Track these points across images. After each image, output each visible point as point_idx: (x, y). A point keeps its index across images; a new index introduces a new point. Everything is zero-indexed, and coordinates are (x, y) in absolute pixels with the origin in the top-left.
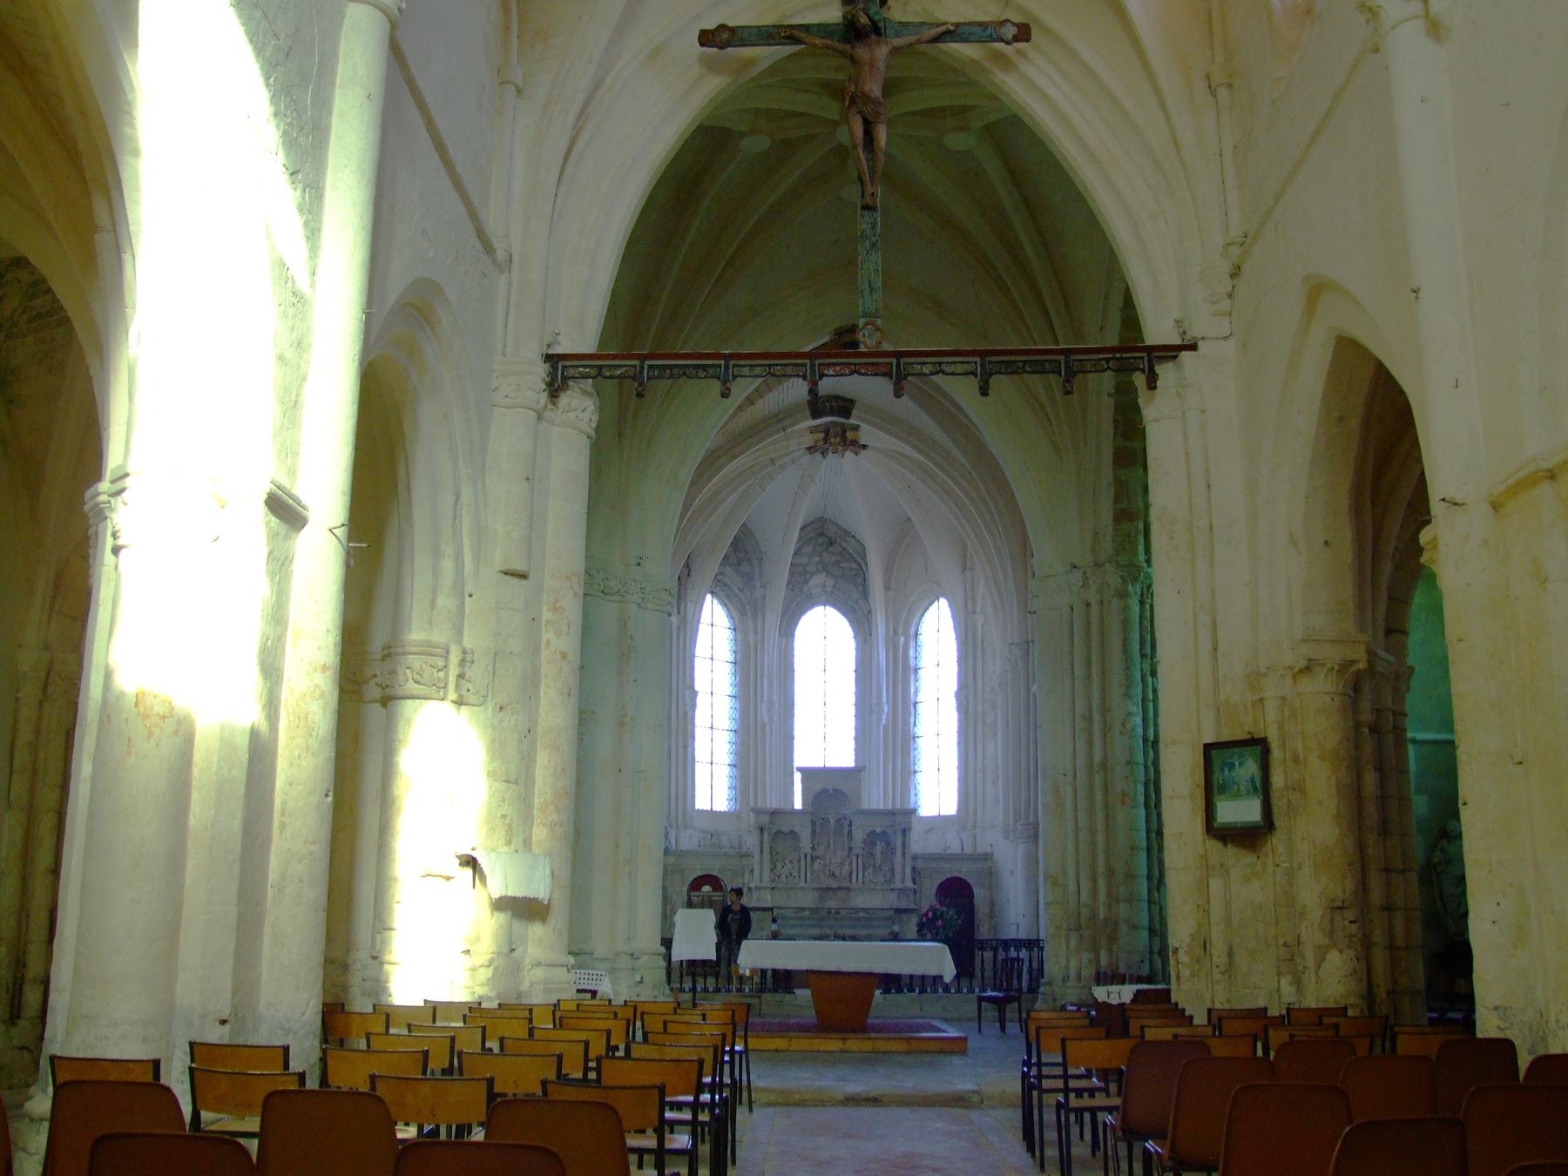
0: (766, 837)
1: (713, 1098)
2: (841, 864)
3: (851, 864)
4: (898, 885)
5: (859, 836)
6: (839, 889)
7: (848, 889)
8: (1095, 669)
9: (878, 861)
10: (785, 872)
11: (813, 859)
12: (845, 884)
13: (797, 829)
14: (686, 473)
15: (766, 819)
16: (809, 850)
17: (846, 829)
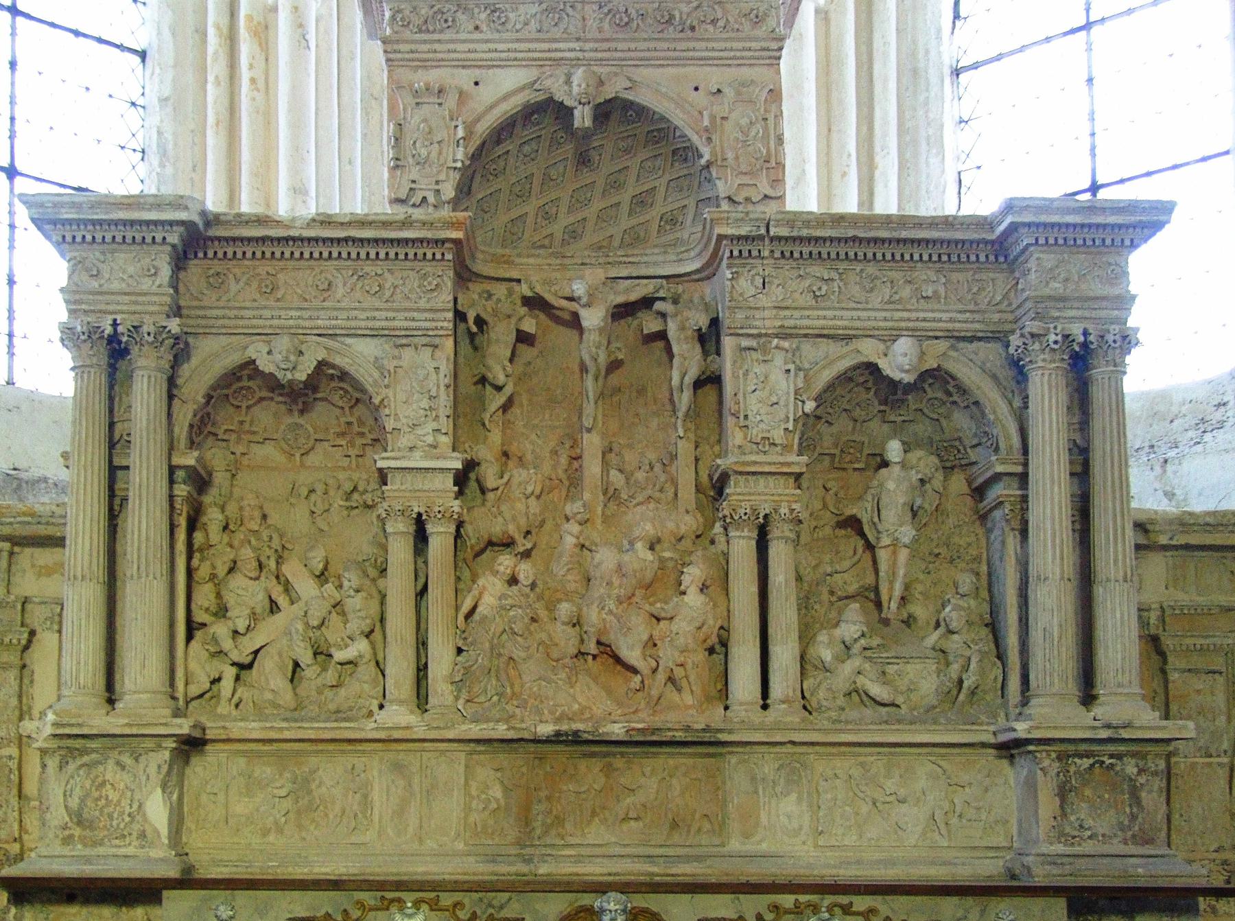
0: (144, 396)
1: (690, 707)
2: (663, 582)
3: (721, 581)
4: (1053, 713)
5: (768, 395)
6: (647, 744)
7: (708, 745)
8: (1114, 407)
9: (897, 568)
10: (282, 636)
11: (472, 552)
12: (686, 711)
13: (361, 356)
14: (479, 609)
15: (142, 280)
16: (439, 493)
17: (688, 360)
